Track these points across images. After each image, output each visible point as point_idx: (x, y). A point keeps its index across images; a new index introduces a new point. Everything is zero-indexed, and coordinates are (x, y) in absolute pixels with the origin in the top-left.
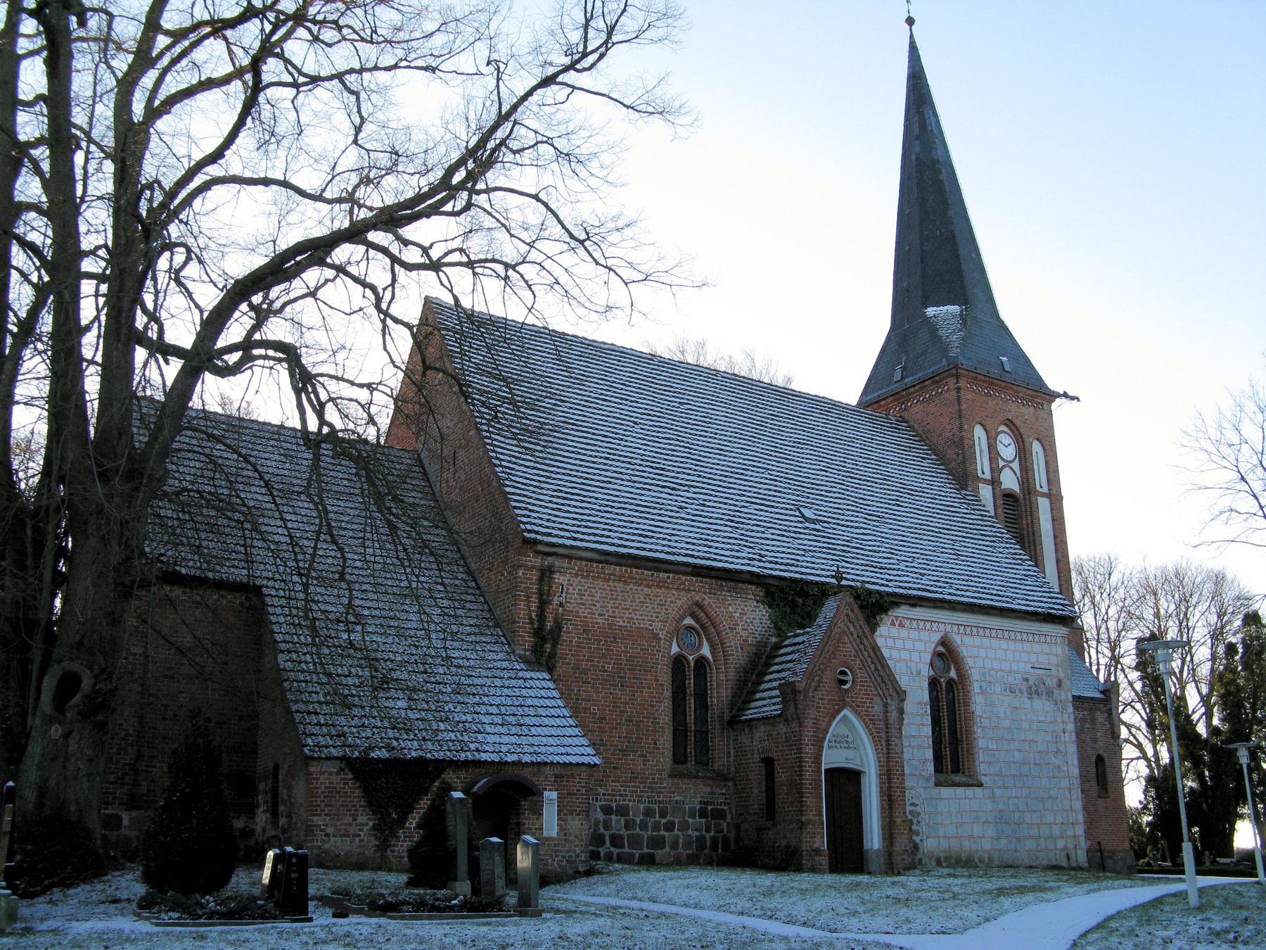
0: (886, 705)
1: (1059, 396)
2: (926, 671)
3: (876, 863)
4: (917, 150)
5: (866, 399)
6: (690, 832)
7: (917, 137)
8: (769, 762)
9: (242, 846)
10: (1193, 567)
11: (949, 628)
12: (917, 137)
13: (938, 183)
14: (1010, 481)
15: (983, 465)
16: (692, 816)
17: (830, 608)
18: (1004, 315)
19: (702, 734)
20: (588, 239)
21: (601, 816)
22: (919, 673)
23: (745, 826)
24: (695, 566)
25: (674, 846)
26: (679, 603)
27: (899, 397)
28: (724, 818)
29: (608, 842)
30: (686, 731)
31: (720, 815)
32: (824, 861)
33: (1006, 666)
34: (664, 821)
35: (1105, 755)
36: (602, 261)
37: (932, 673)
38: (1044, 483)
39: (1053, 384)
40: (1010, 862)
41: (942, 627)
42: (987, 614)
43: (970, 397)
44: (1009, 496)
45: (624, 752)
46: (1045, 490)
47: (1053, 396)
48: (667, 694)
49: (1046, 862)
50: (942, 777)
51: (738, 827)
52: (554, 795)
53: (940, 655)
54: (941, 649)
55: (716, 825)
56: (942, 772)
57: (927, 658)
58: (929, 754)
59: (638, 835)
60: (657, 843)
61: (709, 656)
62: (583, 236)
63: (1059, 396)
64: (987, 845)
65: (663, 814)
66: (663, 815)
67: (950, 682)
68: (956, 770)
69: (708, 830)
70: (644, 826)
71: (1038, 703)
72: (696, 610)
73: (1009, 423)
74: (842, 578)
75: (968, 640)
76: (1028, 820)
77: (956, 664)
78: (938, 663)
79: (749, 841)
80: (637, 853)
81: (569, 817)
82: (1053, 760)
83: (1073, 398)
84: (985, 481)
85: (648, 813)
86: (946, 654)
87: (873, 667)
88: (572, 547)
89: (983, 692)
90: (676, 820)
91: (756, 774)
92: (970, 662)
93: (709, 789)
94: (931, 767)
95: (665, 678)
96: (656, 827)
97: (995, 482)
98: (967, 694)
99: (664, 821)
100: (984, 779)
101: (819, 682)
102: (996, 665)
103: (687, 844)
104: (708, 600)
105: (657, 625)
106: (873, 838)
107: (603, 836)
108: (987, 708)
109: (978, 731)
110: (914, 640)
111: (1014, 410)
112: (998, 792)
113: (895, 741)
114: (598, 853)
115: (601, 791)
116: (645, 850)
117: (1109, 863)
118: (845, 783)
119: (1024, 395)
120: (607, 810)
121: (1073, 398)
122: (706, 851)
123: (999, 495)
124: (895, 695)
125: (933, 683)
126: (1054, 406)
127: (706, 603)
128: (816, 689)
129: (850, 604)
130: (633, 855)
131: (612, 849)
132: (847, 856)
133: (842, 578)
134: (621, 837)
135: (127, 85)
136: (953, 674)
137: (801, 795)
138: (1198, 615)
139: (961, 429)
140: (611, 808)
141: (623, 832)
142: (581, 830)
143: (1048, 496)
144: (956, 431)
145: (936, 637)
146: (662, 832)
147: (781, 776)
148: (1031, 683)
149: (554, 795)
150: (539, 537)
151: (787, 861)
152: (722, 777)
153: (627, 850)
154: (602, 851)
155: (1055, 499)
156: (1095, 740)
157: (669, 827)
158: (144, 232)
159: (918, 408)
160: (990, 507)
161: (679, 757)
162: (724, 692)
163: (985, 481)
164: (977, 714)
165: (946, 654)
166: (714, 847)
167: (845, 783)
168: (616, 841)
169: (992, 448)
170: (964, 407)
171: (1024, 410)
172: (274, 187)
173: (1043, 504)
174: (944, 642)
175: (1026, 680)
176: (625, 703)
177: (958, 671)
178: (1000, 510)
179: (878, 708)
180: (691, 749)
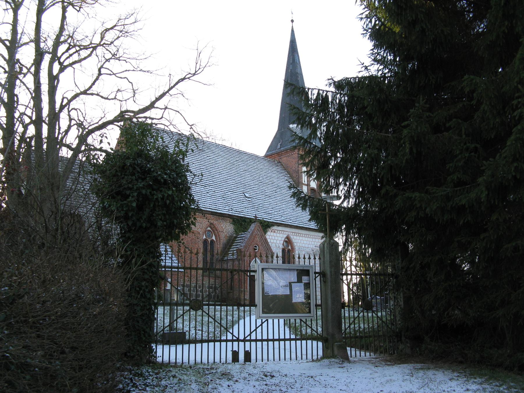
4: (291, 68)
7: (291, 64)
33: (307, 246)
41: (287, 233)
53: (286, 241)
54: (286, 240)
67: (289, 250)
72: (211, 225)
75: (295, 237)
84: (305, 185)
86: (288, 241)
102: (303, 245)
104: (215, 222)
125: (283, 250)
145: (285, 236)
163: (305, 185)
165: (288, 241)
177: (292, 246)
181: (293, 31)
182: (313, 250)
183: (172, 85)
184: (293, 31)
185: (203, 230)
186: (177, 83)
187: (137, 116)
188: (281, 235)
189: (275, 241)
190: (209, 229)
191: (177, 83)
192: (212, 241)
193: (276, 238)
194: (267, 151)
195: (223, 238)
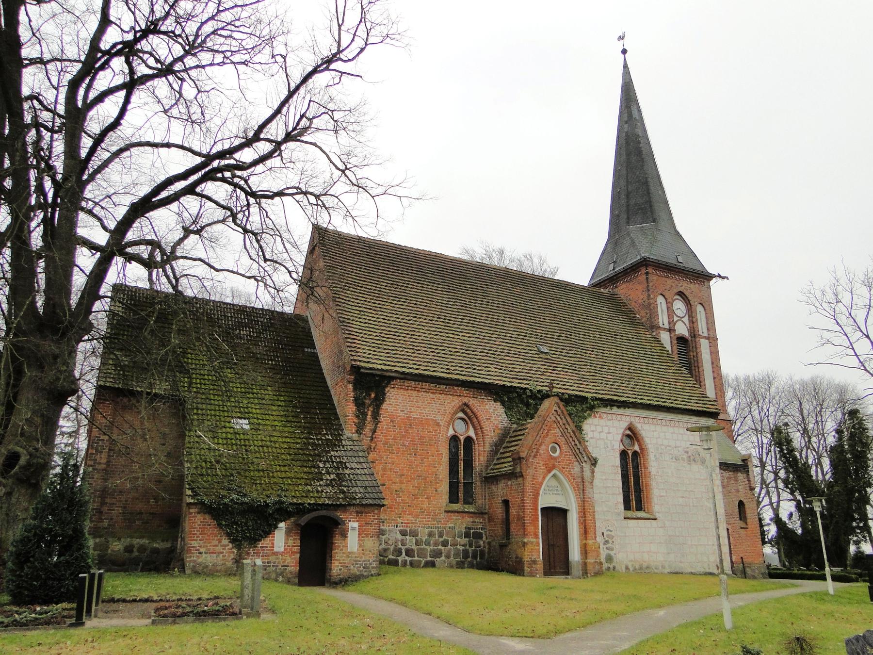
0: (582, 468)
1: (715, 276)
2: (618, 447)
3: (576, 569)
4: (626, 130)
5: (593, 282)
6: (458, 547)
7: (626, 122)
8: (506, 503)
9: (137, 554)
10: (825, 384)
11: (633, 419)
12: (626, 122)
13: (639, 152)
14: (682, 329)
15: (663, 320)
16: (460, 537)
17: (548, 406)
18: (679, 228)
19: (468, 486)
20: (346, 168)
21: (399, 537)
22: (613, 447)
23: (493, 543)
24: (463, 381)
25: (448, 557)
26: (453, 403)
27: (613, 280)
28: (481, 538)
29: (404, 553)
30: (458, 483)
31: (478, 536)
32: (540, 567)
33: (672, 443)
34: (441, 539)
35: (745, 501)
36: (354, 181)
37: (622, 447)
38: (705, 331)
39: (711, 269)
40: (677, 570)
41: (628, 418)
42: (700, 416)
43: (655, 278)
44: (681, 340)
45: (415, 496)
46: (706, 334)
47: (709, 277)
48: (445, 459)
49: (702, 570)
50: (629, 514)
51: (489, 543)
52: (356, 525)
53: (628, 436)
54: (628, 432)
55: (476, 543)
56: (630, 510)
57: (619, 437)
58: (621, 499)
59: (424, 549)
60: (438, 554)
61: (474, 437)
62: (344, 168)
63: (715, 276)
64: (661, 558)
65: (441, 536)
66: (441, 536)
67: (635, 453)
68: (639, 508)
69: (470, 546)
70: (428, 543)
71: (695, 467)
72: (465, 408)
73: (681, 294)
74: (553, 387)
75: (646, 427)
76: (689, 543)
77: (638, 441)
78: (627, 441)
79: (493, 556)
80: (423, 561)
81: (366, 539)
82: (706, 503)
83: (724, 278)
84: (665, 329)
85: (430, 535)
86: (632, 435)
87: (573, 443)
88: (383, 370)
89: (657, 460)
90: (450, 539)
91: (499, 511)
92: (647, 441)
93: (471, 520)
94: (622, 506)
95: (445, 451)
96: (436, 544)
97: (671, 330)
98: (645, 460)
99: (441, 539)
100: (657, 515)
101: (537, 452)
102: (666, 442)
103: (456, 555)
104: (472, 402)
105: (439, 418)
106: (575, 554)
107: (401, 549)
108: (659, 471)
109: (653, 484)
110: (609, 427)
111: (685, 286)
112: (667, 523)
113: (587, 490)
114: (397, 561)
115: (400, 520)
116: (429, 559)
117: (748, 571)
118: (555, 517)
119: (691, 277)
120: (404, 533)
121: (724, 278)
122: (469, 559)
123: (674, 338)
124: (588, 461)
125: (623, 454)
126: (712, 282)
127: (470, 403)
128: (535, 457)
129: (557, 404)
130: (421, 561)
131: (407, 558)
132: (557, 562)
133: (553, 387)
134: (413, 550)
135: (74, 85)
136: (636, 448)
137: (524, 525)
138: (828, 413)
139: (649, 297)
140: (406, 531)
141: (414, 547)
142: (373, 547)
143: (708, 338)
144: (645, 299)
145: (625, 425)
146: (440, 547)
147: (513, 511)
148: (690, 454)
149: (356, 525)
150: (362, 364)
151: (516, 568)
152: (480, 513)
153: (416, 558)
154: (400, 559)
155: (713, 340)
156: (738, 491)
157: (445, 543)
158: (78, 173)
159: (624, 286)
160: (669, 348)
161: (453, 497)
162: (482, 459)
163: (665, 329)
164: (653, 473)
165: (632, 435)
166: (474, 556)
167: (555, 517)
168: (409, 553)
169: (670, 309)
170: (650, 284)
171: (692, 286)
172: (173, 149)
173: (704, 345)
174: (630, 428)
175: (687, 452)
176: (417, 466)
177: (640, 445)
178: (674, 347)
179: (576, 469)
180: (461, 495)
181: (625, 66)
182: (687, 452)
183: (293, 86)
184: (625, 66)
185: (447, 417)
186: (305, 80)
187: (80, 104)
188: (616, 423)
189: (603, 436)
190: (461, 415)
191: (305, 80)
192: (469, 440)
193: (606, 429)
194: (592, 278)
195: (491, 435)
